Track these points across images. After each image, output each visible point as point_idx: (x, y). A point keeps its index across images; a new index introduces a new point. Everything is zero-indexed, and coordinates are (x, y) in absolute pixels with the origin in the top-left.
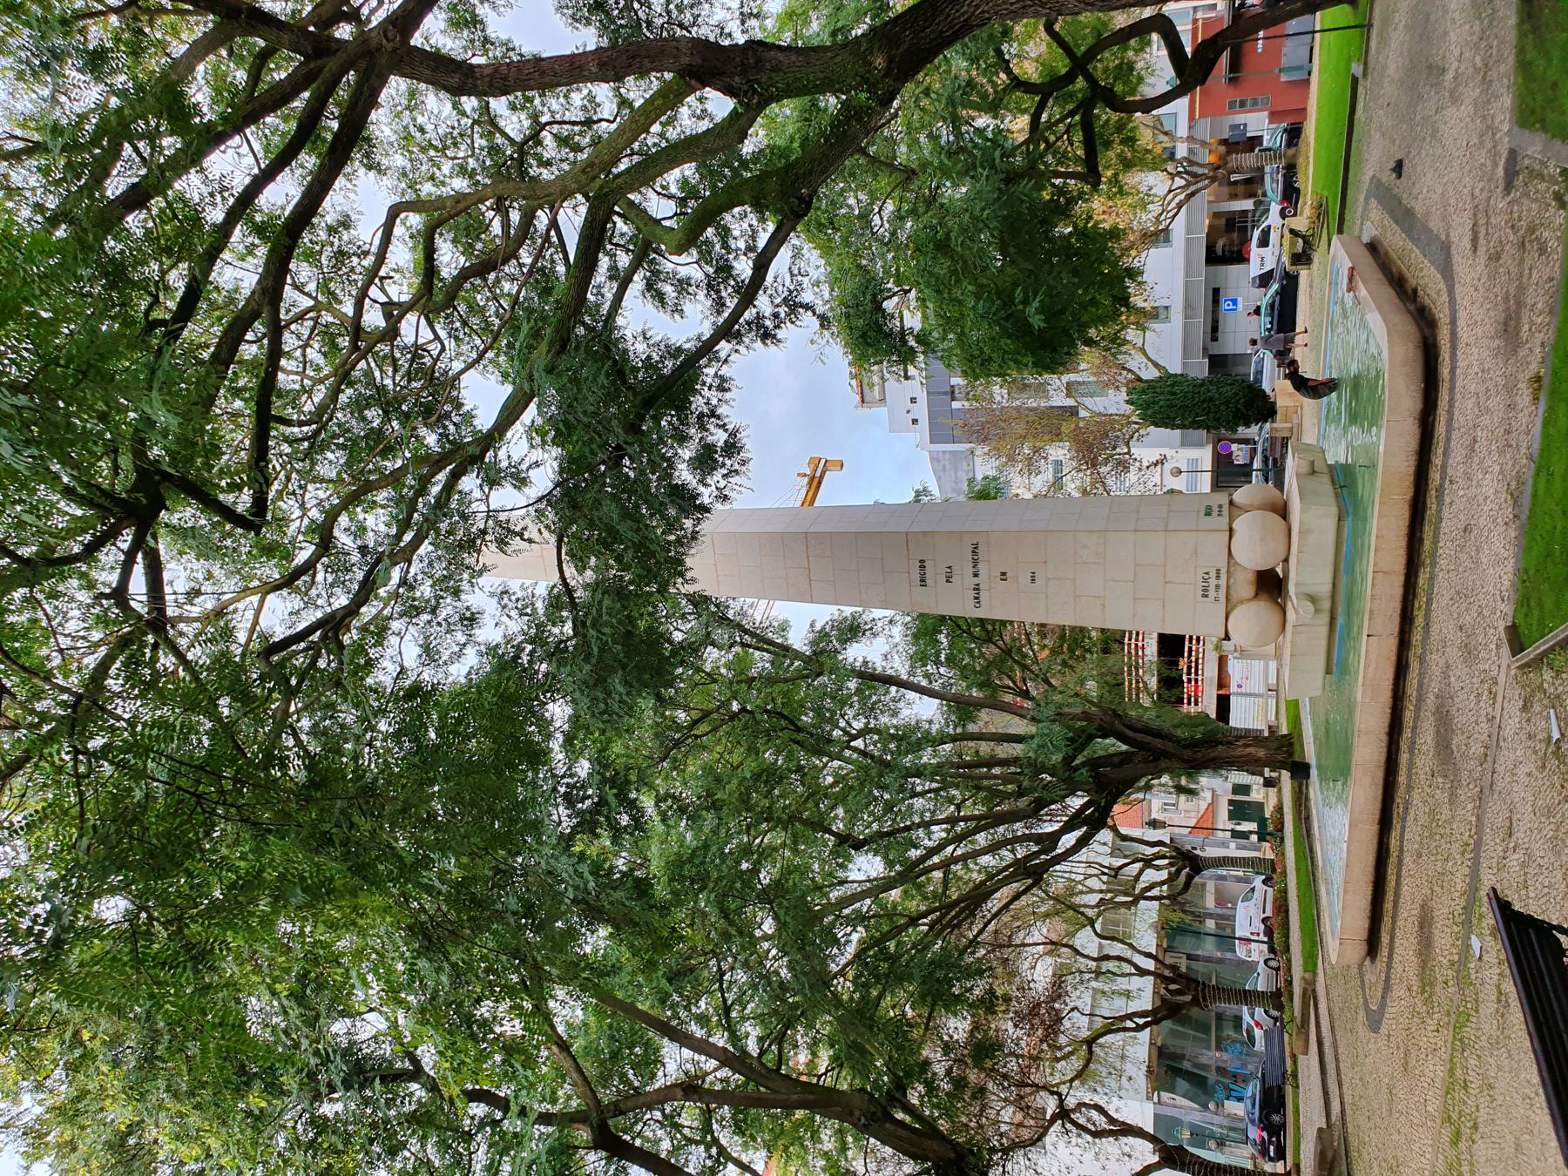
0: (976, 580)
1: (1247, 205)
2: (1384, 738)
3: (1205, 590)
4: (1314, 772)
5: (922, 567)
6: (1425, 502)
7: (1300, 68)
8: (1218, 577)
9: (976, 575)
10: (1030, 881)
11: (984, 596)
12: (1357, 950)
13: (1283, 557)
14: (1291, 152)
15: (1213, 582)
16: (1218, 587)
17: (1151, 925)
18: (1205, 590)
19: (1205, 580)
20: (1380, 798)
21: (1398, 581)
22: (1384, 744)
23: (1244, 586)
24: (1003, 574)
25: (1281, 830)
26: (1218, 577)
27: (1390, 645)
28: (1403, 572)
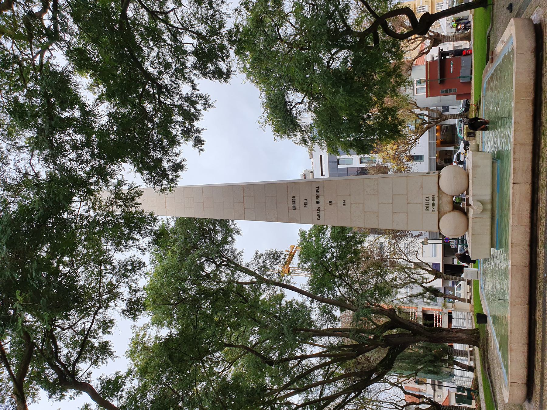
0: (318, 206)
1: (452, 148)
2: (527, 248)
3: (427, 206)
4: (490, 319)
5: (294, 200)
6: (541, 87)
7: (467, 77)
8: (433, 199)
9: (318, 203)
11: (322, 213)
12: (520, 392)
13: (465, 187)
14: (466, 114)
15: (431, 202)
16: (433, 204)
18: (427, 206)
19: (427, 201)
20: (527, 288)
21: (529, 149)
22: (527, 252)
23: (447, 207)
24: (330, 202)
25: (477, 388)
26: (433, 199)
27: (526, 189)
28: (531, 144)
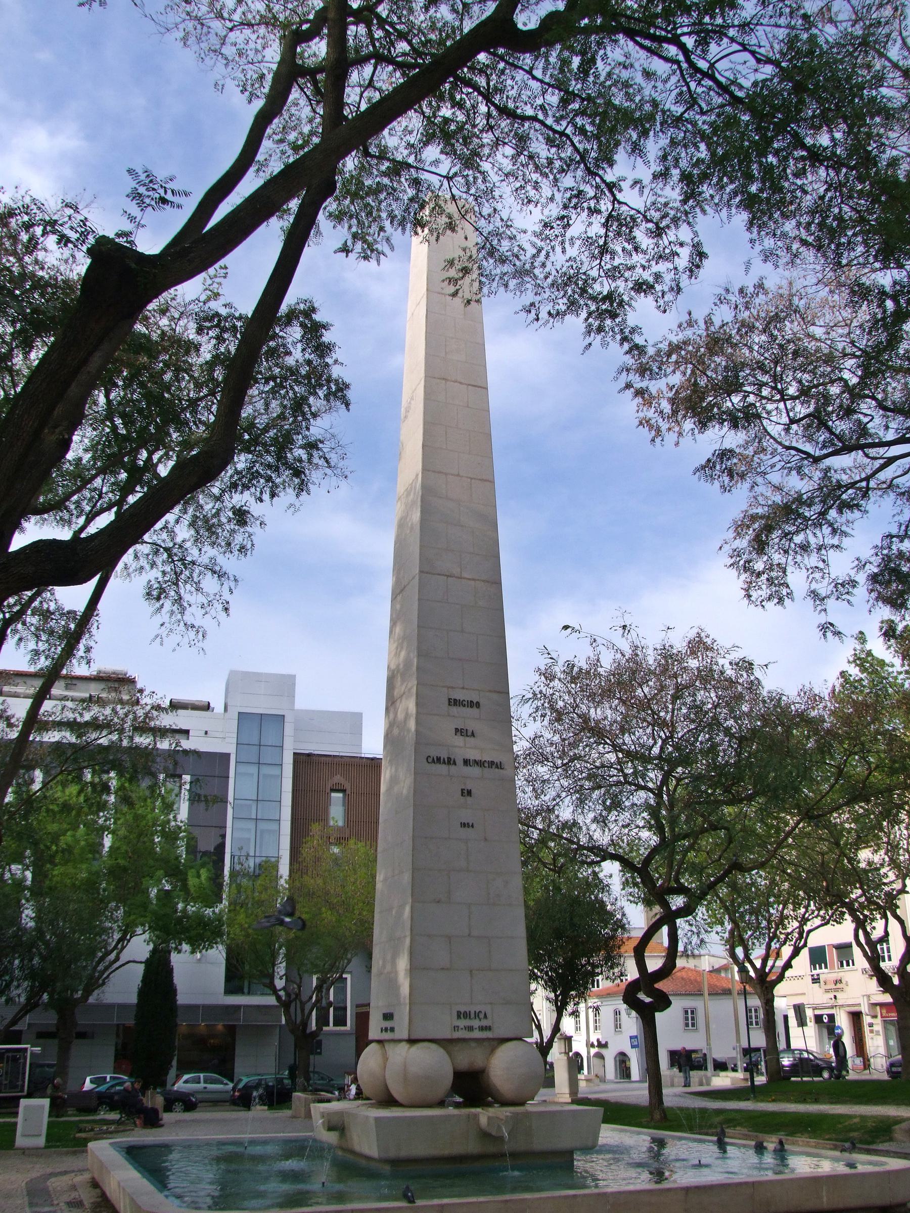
5: (471, 704)
8: (482, 1029)
10: (83, 535)
11: (442, 769)
15: (476, 1023)
16: (470, 1029)
17: (290, 1108)
19: (477, 1015)
23: (468, 1059)
24: (469, 793)
26: (482, 1029)
